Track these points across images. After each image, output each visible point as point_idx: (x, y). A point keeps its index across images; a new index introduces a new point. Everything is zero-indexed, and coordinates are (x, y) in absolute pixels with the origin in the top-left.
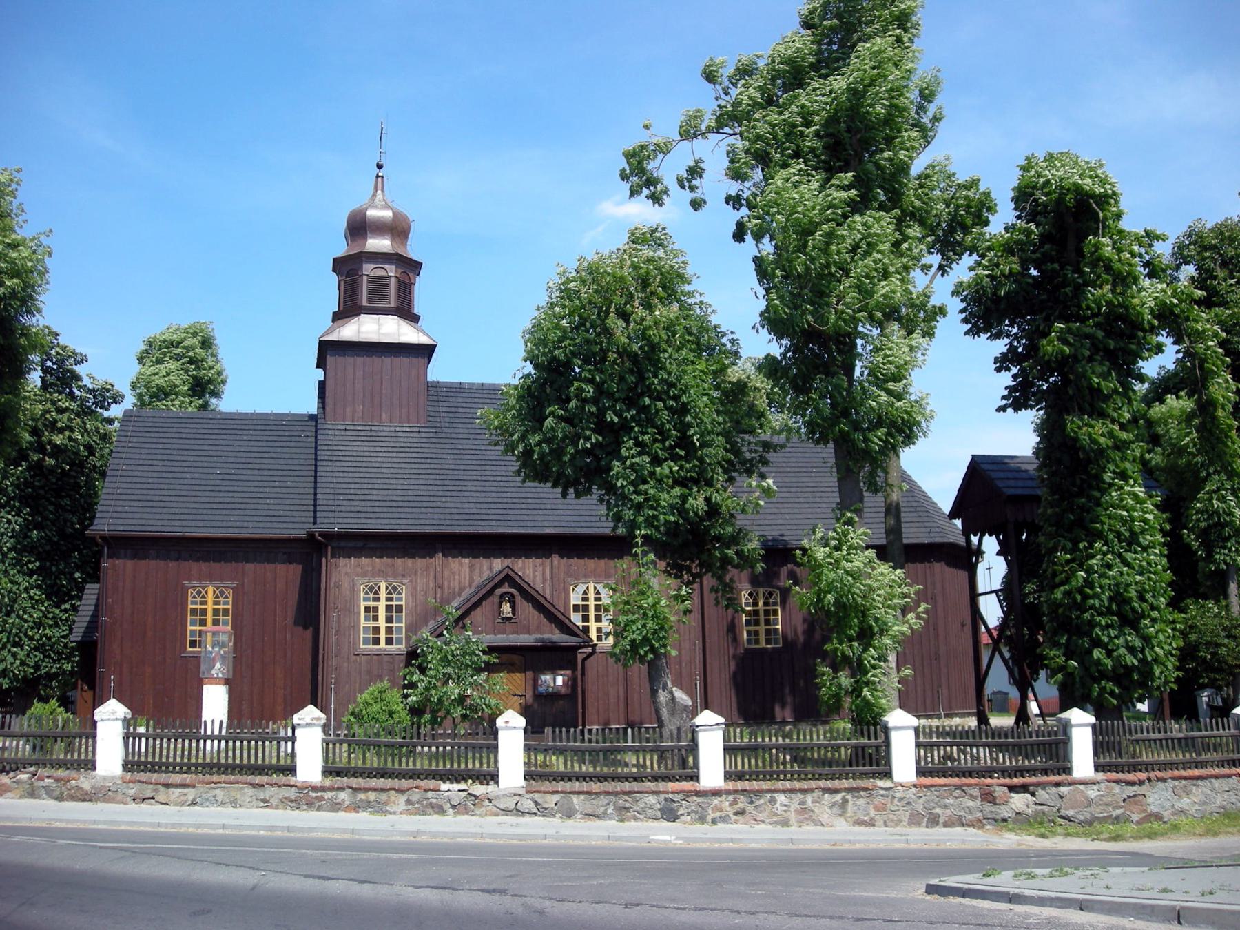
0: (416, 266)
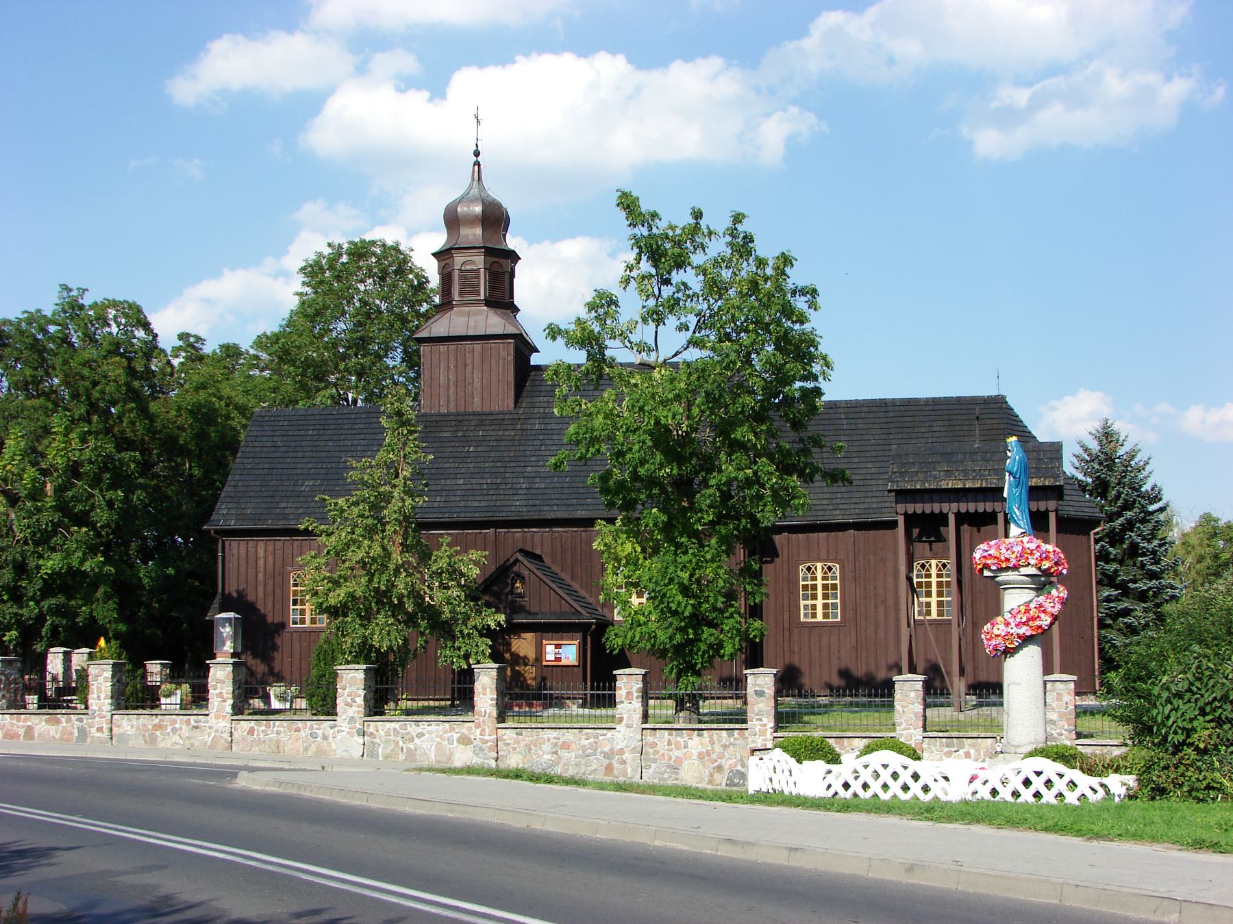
0: (513, 257)
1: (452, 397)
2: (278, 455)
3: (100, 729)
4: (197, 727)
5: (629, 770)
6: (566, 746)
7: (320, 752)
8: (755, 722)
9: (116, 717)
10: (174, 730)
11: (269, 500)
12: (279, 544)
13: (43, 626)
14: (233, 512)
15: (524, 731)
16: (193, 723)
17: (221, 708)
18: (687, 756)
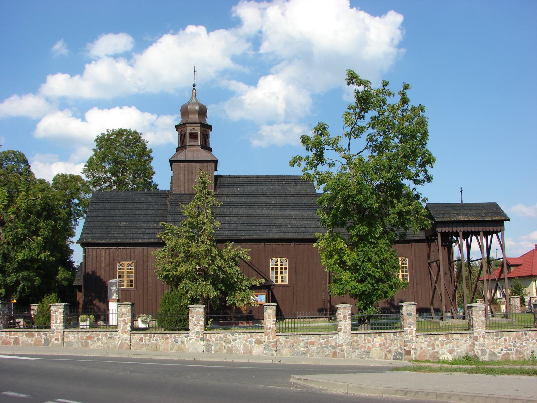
0: (210, 127)
1: (186, 187)
2: (107, 211)
3: (57, 339)
4: (111, 338)
5: (345, 354)
6: (312, 343)
7: (180, 349)
8: (407, 328)
9: (66, 333)
10: (98, 339)
11: (106, 230)
12: (112, 250)
13: (18, 286)
14: (90, 235)
15: (290, 337)
16: (108, 335)
18: (373, 346)
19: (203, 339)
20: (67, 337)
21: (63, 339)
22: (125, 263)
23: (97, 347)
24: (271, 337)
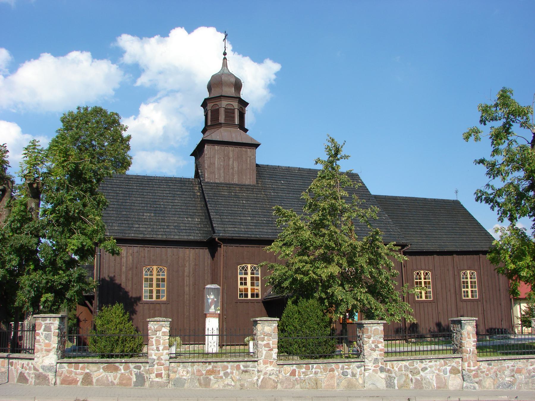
0: (245, 104)
3: (159, 375)
4: (246, 371)
6: (519, 371)
9: (173, 364)
10: (226, 374)
15: (493, 363)
16: (242, 368)
17: (269, 356)
19: (382, 370)
20: (175, 372)
21: (169, 376)
22: (155, 268)
23: (224, 386)
24: (472, 363)
